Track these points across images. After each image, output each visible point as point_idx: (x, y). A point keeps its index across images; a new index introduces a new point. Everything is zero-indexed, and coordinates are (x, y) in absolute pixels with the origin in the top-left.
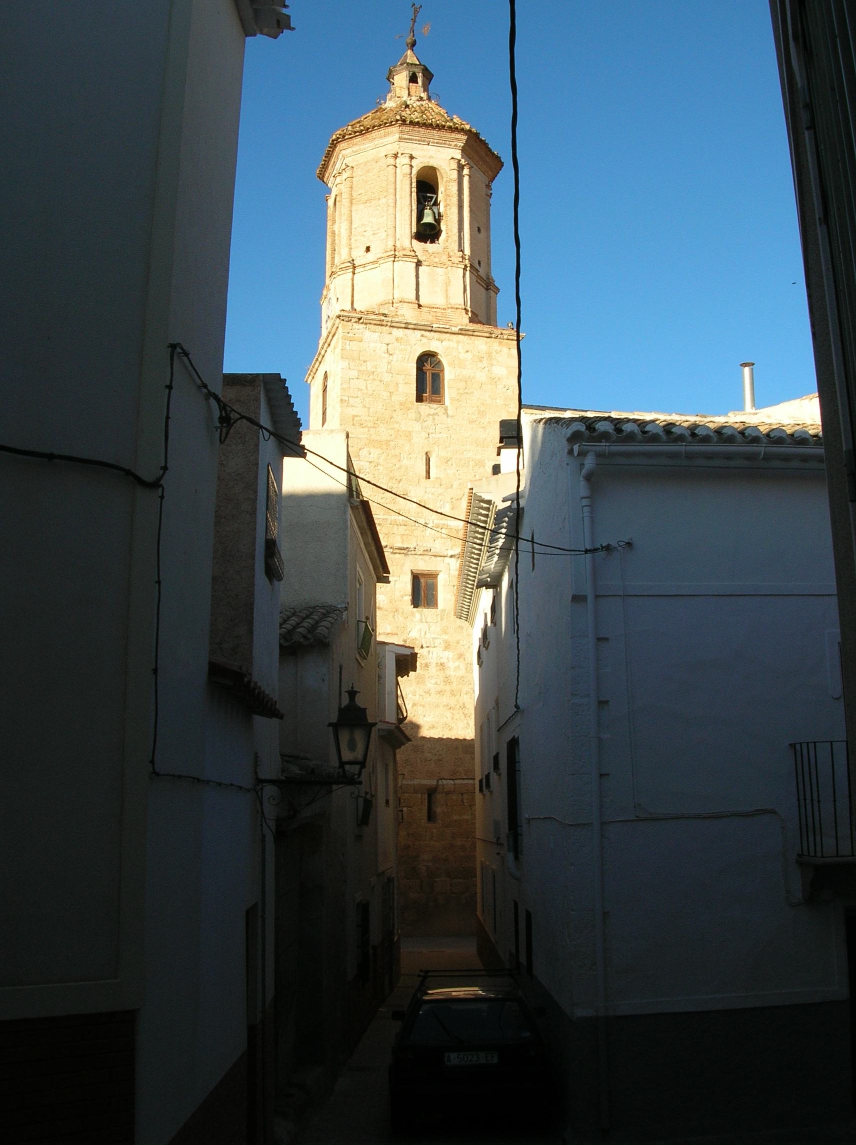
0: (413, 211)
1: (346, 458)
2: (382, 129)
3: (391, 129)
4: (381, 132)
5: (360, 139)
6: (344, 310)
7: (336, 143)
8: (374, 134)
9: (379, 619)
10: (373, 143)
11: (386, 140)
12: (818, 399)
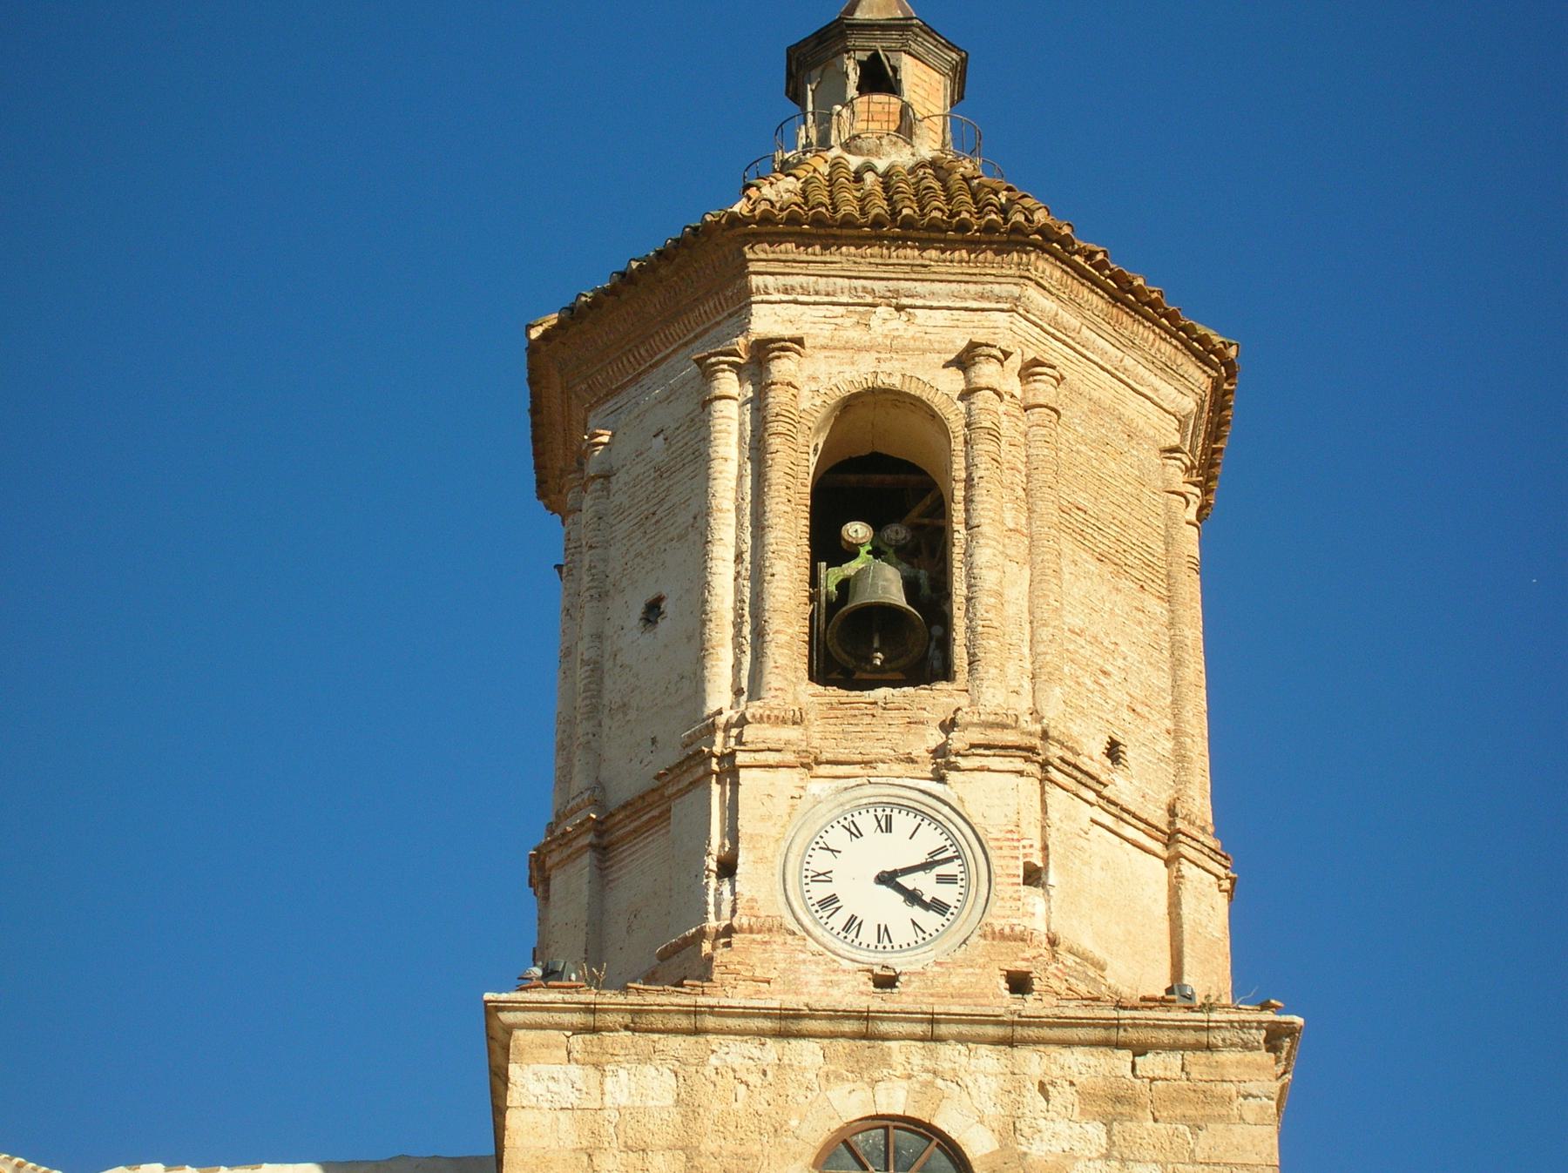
0: (967, 924)
1: (531, 461)
2: (1175, 342)
3: (1191, 368)
4: (1164, 346)
5: (1101, 304)
6: (887, 967)
7: (1036, 246)
8: (1144, 333)
9: (921, 1109)
10: (1120, 354)
11: (1157, 382)
12: (902, 1113)
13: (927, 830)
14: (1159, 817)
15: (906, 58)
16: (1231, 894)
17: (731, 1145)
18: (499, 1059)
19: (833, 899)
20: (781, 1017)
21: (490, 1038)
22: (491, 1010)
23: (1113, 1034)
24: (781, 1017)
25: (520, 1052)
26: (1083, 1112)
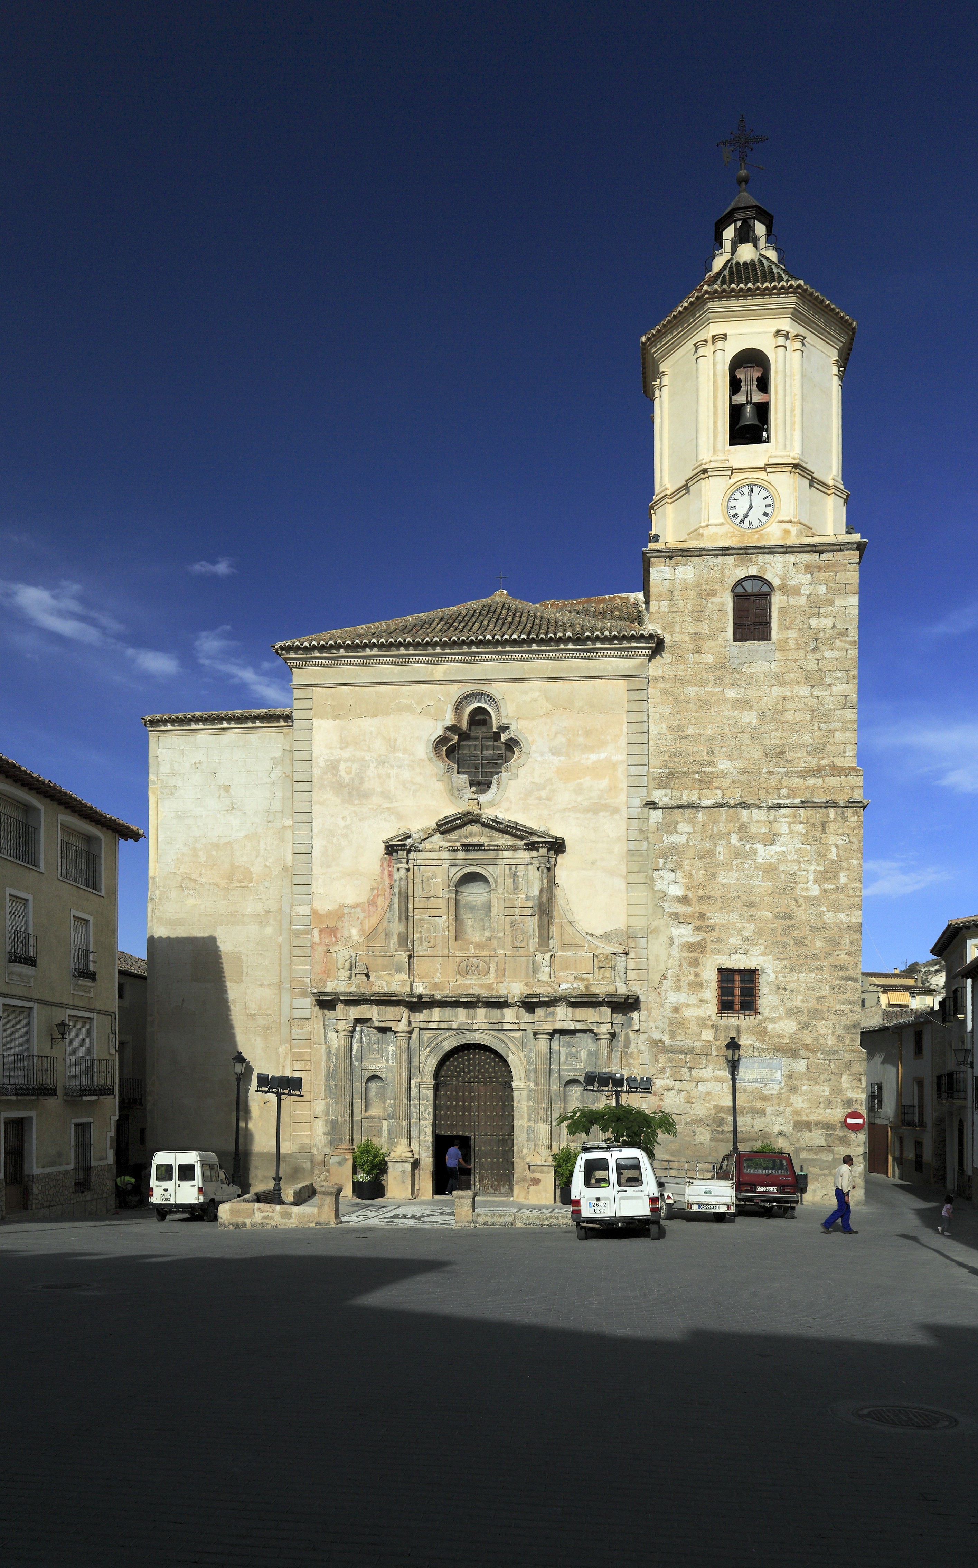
13: (763, 491)
14: (663, 385)
15: (756, 222)
16: (846, 501)
17: (708, 587)
18: (646, 567)
19: (736, 514)
20: (723, 550)
21: (644, 561)
22: (644, 553)
23: (814, 549)
24: (723, 550)
25: (653, 564)
26: (805, 571)
